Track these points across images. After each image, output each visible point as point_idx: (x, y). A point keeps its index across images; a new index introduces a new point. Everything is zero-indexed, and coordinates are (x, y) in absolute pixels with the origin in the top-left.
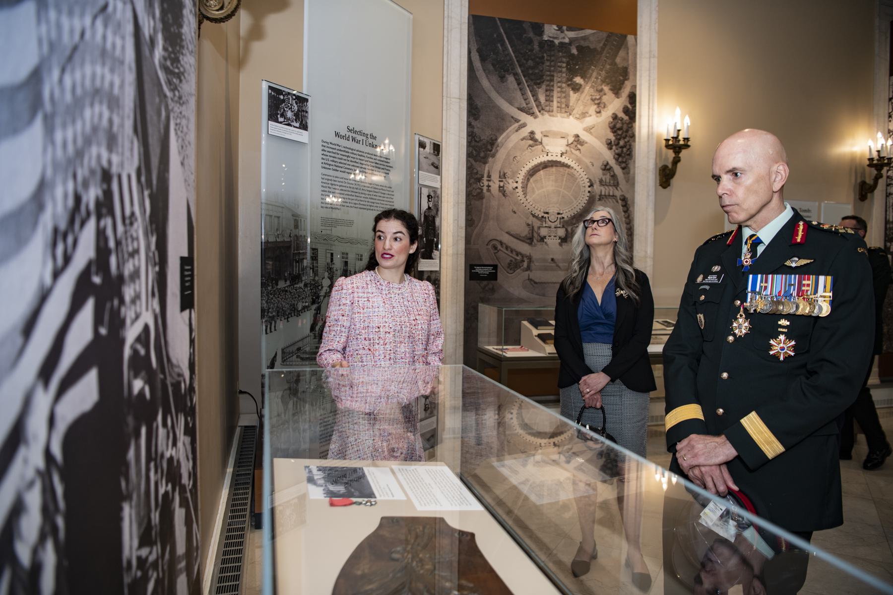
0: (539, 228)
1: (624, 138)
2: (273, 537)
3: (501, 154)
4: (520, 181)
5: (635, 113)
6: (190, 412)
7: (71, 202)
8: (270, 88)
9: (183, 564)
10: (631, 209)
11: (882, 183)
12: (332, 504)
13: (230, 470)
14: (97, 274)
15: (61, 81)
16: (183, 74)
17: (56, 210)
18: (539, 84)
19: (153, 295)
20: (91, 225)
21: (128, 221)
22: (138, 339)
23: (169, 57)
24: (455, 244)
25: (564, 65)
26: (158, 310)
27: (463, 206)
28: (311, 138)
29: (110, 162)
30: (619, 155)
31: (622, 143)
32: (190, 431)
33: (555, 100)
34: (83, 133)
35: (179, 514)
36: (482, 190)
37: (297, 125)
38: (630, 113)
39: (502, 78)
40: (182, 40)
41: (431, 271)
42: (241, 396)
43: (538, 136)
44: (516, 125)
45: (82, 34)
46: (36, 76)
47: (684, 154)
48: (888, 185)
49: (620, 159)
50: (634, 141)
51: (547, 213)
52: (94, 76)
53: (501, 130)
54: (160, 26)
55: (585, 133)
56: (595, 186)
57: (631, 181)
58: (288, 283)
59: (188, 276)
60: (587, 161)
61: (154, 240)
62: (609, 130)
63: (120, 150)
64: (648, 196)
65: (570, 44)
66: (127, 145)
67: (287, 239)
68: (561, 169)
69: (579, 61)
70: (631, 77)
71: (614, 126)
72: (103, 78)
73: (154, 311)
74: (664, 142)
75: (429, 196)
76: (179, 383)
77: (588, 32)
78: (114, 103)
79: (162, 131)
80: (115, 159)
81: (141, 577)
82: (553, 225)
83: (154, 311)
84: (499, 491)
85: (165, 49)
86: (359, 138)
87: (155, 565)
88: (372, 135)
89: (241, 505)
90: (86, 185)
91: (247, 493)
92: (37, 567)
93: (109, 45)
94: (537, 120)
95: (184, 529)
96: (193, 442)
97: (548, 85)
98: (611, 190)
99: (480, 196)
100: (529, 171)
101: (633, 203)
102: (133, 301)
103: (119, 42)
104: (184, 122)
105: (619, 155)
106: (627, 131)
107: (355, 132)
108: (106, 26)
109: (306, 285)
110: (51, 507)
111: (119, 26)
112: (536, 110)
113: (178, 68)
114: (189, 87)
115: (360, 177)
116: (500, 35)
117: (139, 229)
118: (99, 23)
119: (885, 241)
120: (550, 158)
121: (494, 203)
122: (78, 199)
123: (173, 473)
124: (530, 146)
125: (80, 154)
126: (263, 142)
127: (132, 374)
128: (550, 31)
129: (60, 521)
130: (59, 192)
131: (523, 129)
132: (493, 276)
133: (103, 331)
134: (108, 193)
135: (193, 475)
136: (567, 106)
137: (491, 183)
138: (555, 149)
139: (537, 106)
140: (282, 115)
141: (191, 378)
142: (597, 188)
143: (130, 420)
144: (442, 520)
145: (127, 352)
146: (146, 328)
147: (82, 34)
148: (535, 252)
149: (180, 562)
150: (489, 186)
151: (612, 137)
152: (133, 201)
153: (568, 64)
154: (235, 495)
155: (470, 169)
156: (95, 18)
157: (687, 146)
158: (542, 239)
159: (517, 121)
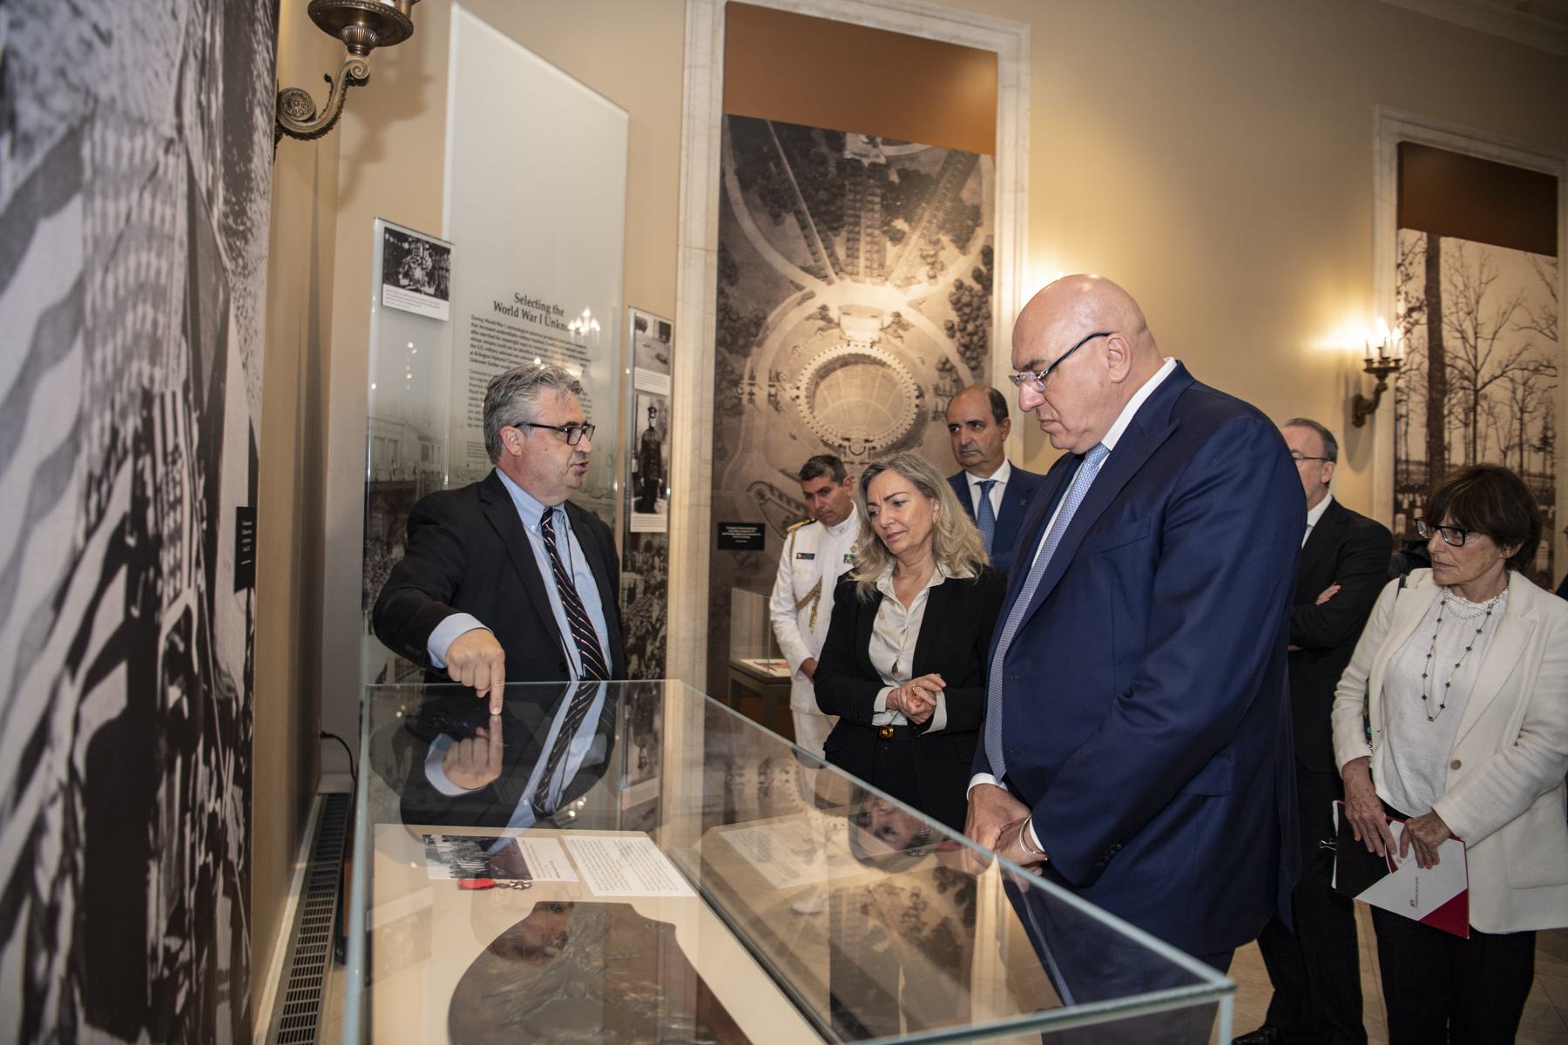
1: (975, 320)
2: (368, 982)
3: (773, 342)
4: (803, 386)
6: (244, 750)
7: (107, 439)
8: (387, 230)
9: (225, 987)
11: (1387, 398)
12: (462, 887)
13: (301, 866)
14: (131, 534)
15: (103, 285)
16: (250, 230)
18: (836, 229)
21: (170, 459)
22: (176, 628)
24: (695, 487)
25: (878, 200)
26: (203, 587)
27: (709, 427)
28: (452, 312)
29: (152, 379)
30: (966, 347)
31: (970, 327)
32: (243, 780)
33: (862, 255)
34: (124, 346)
35: (223, 906)
37: (431, 290)
38: (985, 279)
39: (776, 218)
40: (250, 180)
41: (653, 534)
42: (325, 742)
43: (834, 314)
44: (798, 295)
46: (79, 287)
48: (1398, 402)
49: (968, 354)
50: (991, 325)
51: (848, 440)
53: (773, 302)
54: (221, 169)
55: (910, 310)
56: (927, 397)
59: (247, 536)
60: (914, 356)
62: (949, 306)
63: (165, 360)
65: (888, 165)
66: (173, 351)
67: (408, 477)
68: (871, 368)
69: (901, 192)
70: (986, 221)
72: (148, 265)
73: (198, 587)
75: (651, 410)
76: (229, 701)
77: (917, 147)
78: (159, 297)
80: (158, 373)
81: (169, 979)
83: (198, 587)
84: (760, 907)
85: (227, 202)
86: (535, 312)
87: (187, 967)
89: (321, 911)
90: (124, 415)
91: (330, 902)
92: (54, 910)
94: (833, 287)
95: (229, 932)
96: (247, 798)
97: (850, 232)
99: (737, 410)
100: (818, 371)
102: (172, 573)
105: (966, 347)
106: (979, 308)
107: (529, 303)
108: (154, 196)
110: (72, 836)
112: (830, 271)
114: (258, 247)
116: (773, 149)
117: (183, 469)
118: (147, 196)
119: (1396, 492)
120: (852, 350)
121: (760, 422)
122: (115, 433)
123: (215, 838)
124: (821, 329)
125: (119, 374)
128: (855, 144)
129: (80, 858)
130: (95, 426)
133: (135, 612)
134: (148, 422)
135: (245, 849)
136: (882, 266)
137: (755, 390)
138: (860, 335)
139: (833, 265)
140: (406, 275)
141: (247, 697)
142: (931, 401)
143: (163, 743)
144: (628, 907)
145: (162, 645)
146: (187, 612)
149: (222, 982)
150: (751, 394)
151: (954, 317)
152: (179, 431)
153: (883, 197)
154: (309, 904)
155: (721, 365)
159: (799, 288)
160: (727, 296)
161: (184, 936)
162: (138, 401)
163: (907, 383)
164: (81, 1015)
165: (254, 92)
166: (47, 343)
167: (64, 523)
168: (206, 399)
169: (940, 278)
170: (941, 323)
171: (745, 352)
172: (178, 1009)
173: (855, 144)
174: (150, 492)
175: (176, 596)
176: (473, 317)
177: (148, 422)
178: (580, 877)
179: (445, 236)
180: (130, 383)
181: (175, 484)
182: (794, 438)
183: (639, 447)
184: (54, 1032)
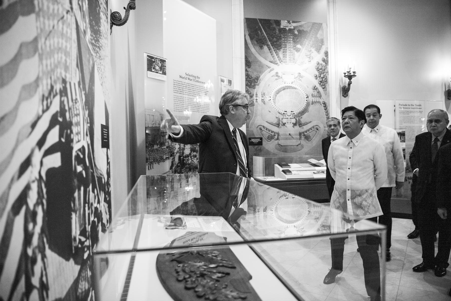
0: (282, 119)
4: (272, 96)
5: (328, 61)
7: (49, 87)
8: (148, 56)
15: (45, 43)
17: (44, 88)
18: (279, 49)
19: (87, 135)
21: (74, 101)
22: (79, 150)
23: (94, 39)
25: (292, 39)
26: (89, 142)
29: (66, 76)
32: (108, 202)
33: (288, 56)
34: (54, 63)
38: (326, 61)
39: (261, 47)
40: (100, 32)
43: (280, 74)
44: (269, 70)
45: (53, 27)
46: (36, 40)
47: (353, 80)
49: (322, 84)
50: (328, 75)
52: (58, 43)
53: (261, 72)
54: (88, 26)
56: (309, 97)
57: (327, 95)
58: (159, 146)
61: (87, 113)
62: (315, 70)
64: (337, 101)
65: (294, 29)
66: (73, 71)
68: (292, 90)
70: (325, 43)
71: (318, 68)
72: (62, 44)
78: (67, 54)
79: (91, 69)
80: (68, 76)
82: (289, 117)
86: (191, 78)
87: (88, 247)
88: (198, 77)
90: (55, 82)
92: (34, 214)
93: (65, 32)
98: (318, 99)
103: (69, 31)
104: (102, 67)
106: (324, 70)
108: (63, 24)
109: (167, 147)
110: (41, 194)
111: (69, 25)
112: (278, 62)
113: (98, 44)
114: (106, 51)
118: (60, 23)
120: (286, 85)
121: (259, 108)
122: (52, 87)
123: (98, 214)
125: (53, 71)
127: (76, 163)
128: (284, 24)
129: (45, 202)
130: (45, 82)
132: (260, 143)
133: (63, 140)
136: (294, 59)
137: (257, 98)
138: (288, 80)
139: (279, 60)
140: (154, 68)
142: (311, 99)
147: (53, 27)
148: (281, 131)
150: (257, 100)
151: (317, 73)
152: (77, 94)
153: (293, 39)
156: (58, 21)
158: (284, 124)
159: (269, 67)
160: (248, 71)
161: (87, 238)
164: (47, 246)
165: (100, 8)
166: (24, 51)
169: (312, 61)
171: (254, 87)
173: (284, 24)
179: (164, 57)
181: (77, 109)
184: (36, 247)
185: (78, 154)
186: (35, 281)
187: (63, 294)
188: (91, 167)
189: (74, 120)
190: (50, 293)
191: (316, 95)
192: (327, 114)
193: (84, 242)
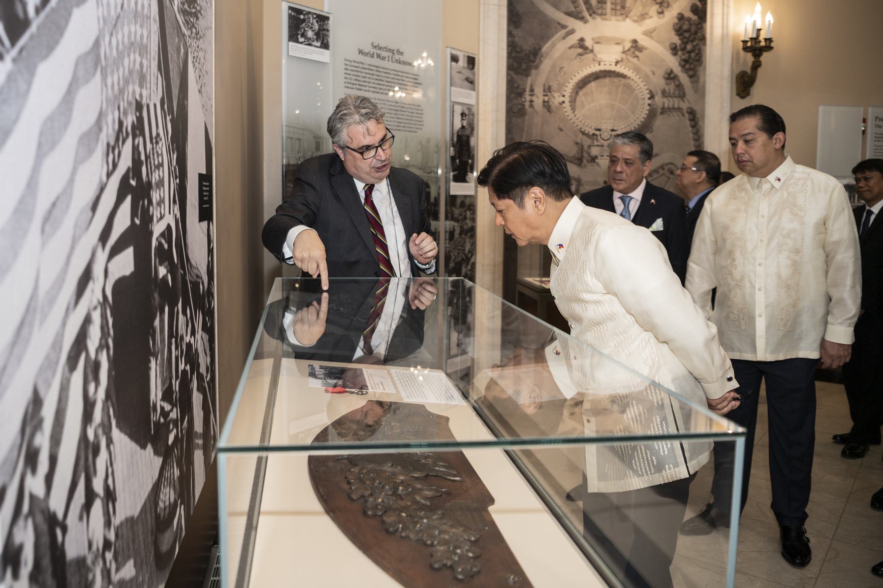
0: (589, 147)
1: (692, 41)
3: (546, 65)
4: (567, 94)
8: (290, 8)
10: (700, 123)
12: (327, 391)
15: (110, 42)
16: (200, 12)
20: (129, 141)
22: (162, 235)
26: (178, 216)
29: (141, 96)
32: (209, 330)
35: (197, 398)
36: (524, 106)
37: (319, 44)
41: (466, 196)
43: (589, 43)
44: (563, 32)
47: (765, 57)
49: (687, 66)
50: (705, 44)
51: (599, 130)
53: (545, 38)
55: (645, 37)
56: (657, 98)
57: (700, 91)
60: (647, 70)
62: (673, 33)
66: (153, 81)
68: (616, 80)
72: (136, 33)
74: (741, 44)
75: (463, 114)
80: (145, 93)
86: (384, 54)
87: (175, 422)
88: (398, 51)
90: (125, 113)
92: (97, 365)
94: (587, 25)
95: (202, 413)
96: (211, 341)
98: (676, 103)
100: (577, 84)
101: (703, 116)
104: (201, 54)
105: (686, 61)
106: (696, 33)
107: (380, 48)
110: (106, 330)
112: (586, 14)
113: (194, 7)
115: (400, 95)
117: (163, 147)
122: (121, 124)
123: (191, 357)
124: (580, 55)
125: (121, 91)
126: (284, 61)
131: (571, 36)
133: (137, 222)
134: (140, 119)
135: (211, 368)
136: (623, 7)
137: (534, 98)
138: (608, 57)
139: (588, 10)
140: (303, 35)
142: (659, 100)
144: (424, 406)
146: (169, 227)
150: (531, 101)
151: (676, 40)
152: (160, 126)
157: (768, 48)
158: (593, 159)
159: (564, 27)
162: (134, 107)
163: (642, 89)
167: (94, 168)
168: (175, 109)
170: (667, 45)
171: (526, 73)
172: (170, 443)
174: (143, 158)
175: (162, 217)
176: (346, 60)
177: (140, 119)
178: (398, 391)
179: (326, 9)
180: (128, 96)
182: (561, 130)
183: (455, 139)
184: (99, 425)
185: (160, 244)
186: (98, 486)
187: (136, 511)
188: (180, 262)
189: (155, 178)
190: (118, 505)
191: (672, 91)
192: (698, 136)
193: (168, 413)
